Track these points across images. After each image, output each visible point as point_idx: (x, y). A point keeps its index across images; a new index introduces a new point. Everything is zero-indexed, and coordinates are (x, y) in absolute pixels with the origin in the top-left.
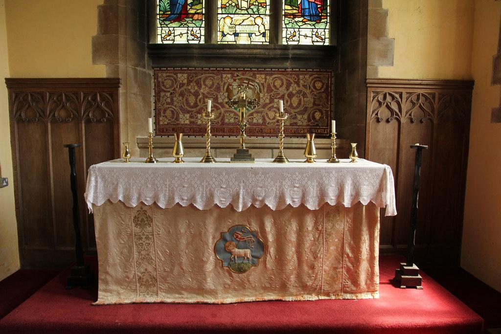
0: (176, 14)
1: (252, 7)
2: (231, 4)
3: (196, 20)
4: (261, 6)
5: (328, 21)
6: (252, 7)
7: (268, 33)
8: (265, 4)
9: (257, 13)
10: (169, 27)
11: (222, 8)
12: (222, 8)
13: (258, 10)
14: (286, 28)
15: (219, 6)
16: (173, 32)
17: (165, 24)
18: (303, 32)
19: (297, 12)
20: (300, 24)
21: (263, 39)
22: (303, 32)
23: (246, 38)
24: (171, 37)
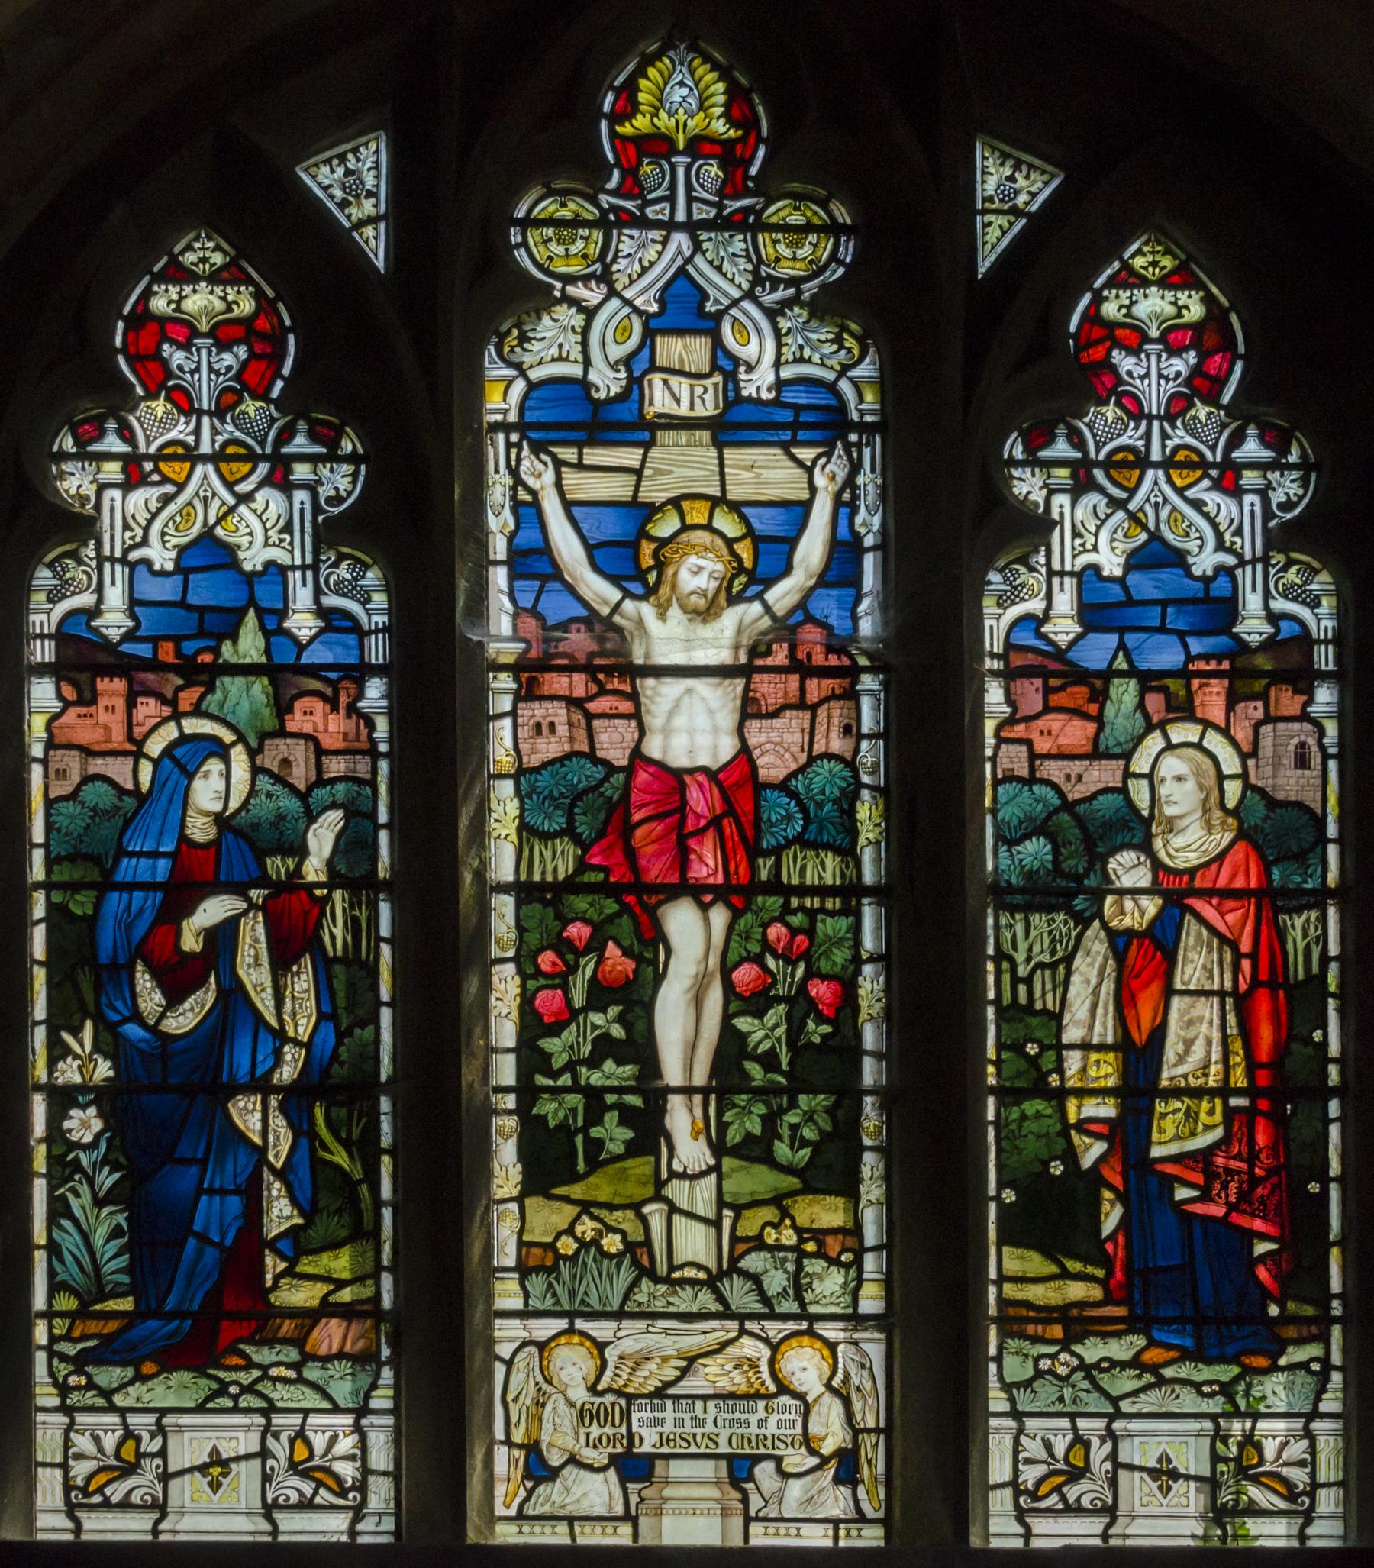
0: (178, 1314)
1: (753, 1262)
2: (595, 1242)
3: (327, 1359)
4: (820, 1254)
5: (1336, 1358)
6: (753, 1262)
7: (874, 1455)
8: (851, 1242)
9: (789, 1306)
10: (123, 1412)
11: (523, 1270)
12: (523, 1270)
13: (798, 1286)
14: (1016, 1414)
15: (507, 1255)
16: (155, 1446)
17: (91, 1385)
18: (1142, 1448)
19: (1096, 1293)
20: (1124, 1382)
21: (837, 1502)
22: (1142, 1448)
23: (713, 1492)
24: (142, 1484)
